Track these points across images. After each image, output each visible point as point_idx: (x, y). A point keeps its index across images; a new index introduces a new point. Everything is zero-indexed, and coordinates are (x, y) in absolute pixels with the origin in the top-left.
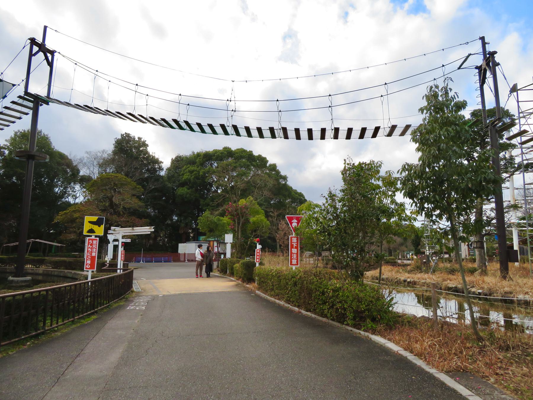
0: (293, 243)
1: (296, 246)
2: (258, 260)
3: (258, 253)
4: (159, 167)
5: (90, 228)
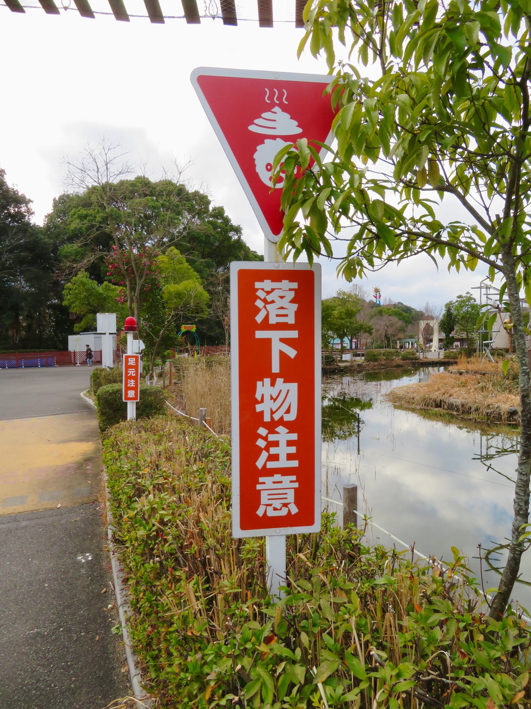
0: (266, 325)
1: (292, 353)
2: (131, 393)
3: (131, 367)
4: (28, 209)
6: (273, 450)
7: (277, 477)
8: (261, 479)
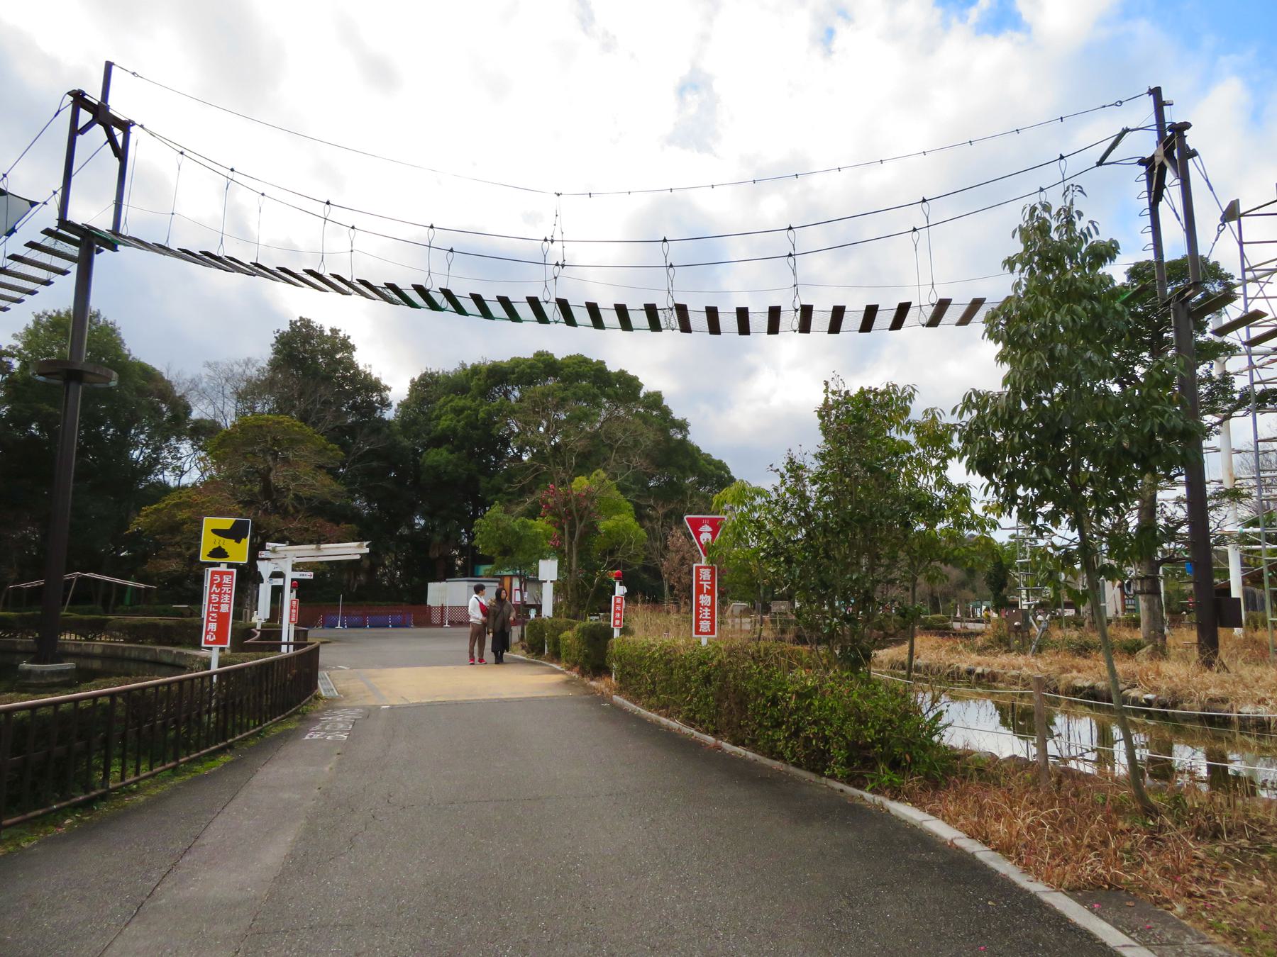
0: (702, 580)
1: (709, 588)
2: (618, 622)
3: (618, 604)
4: (382, 398)
5: (216, 546)
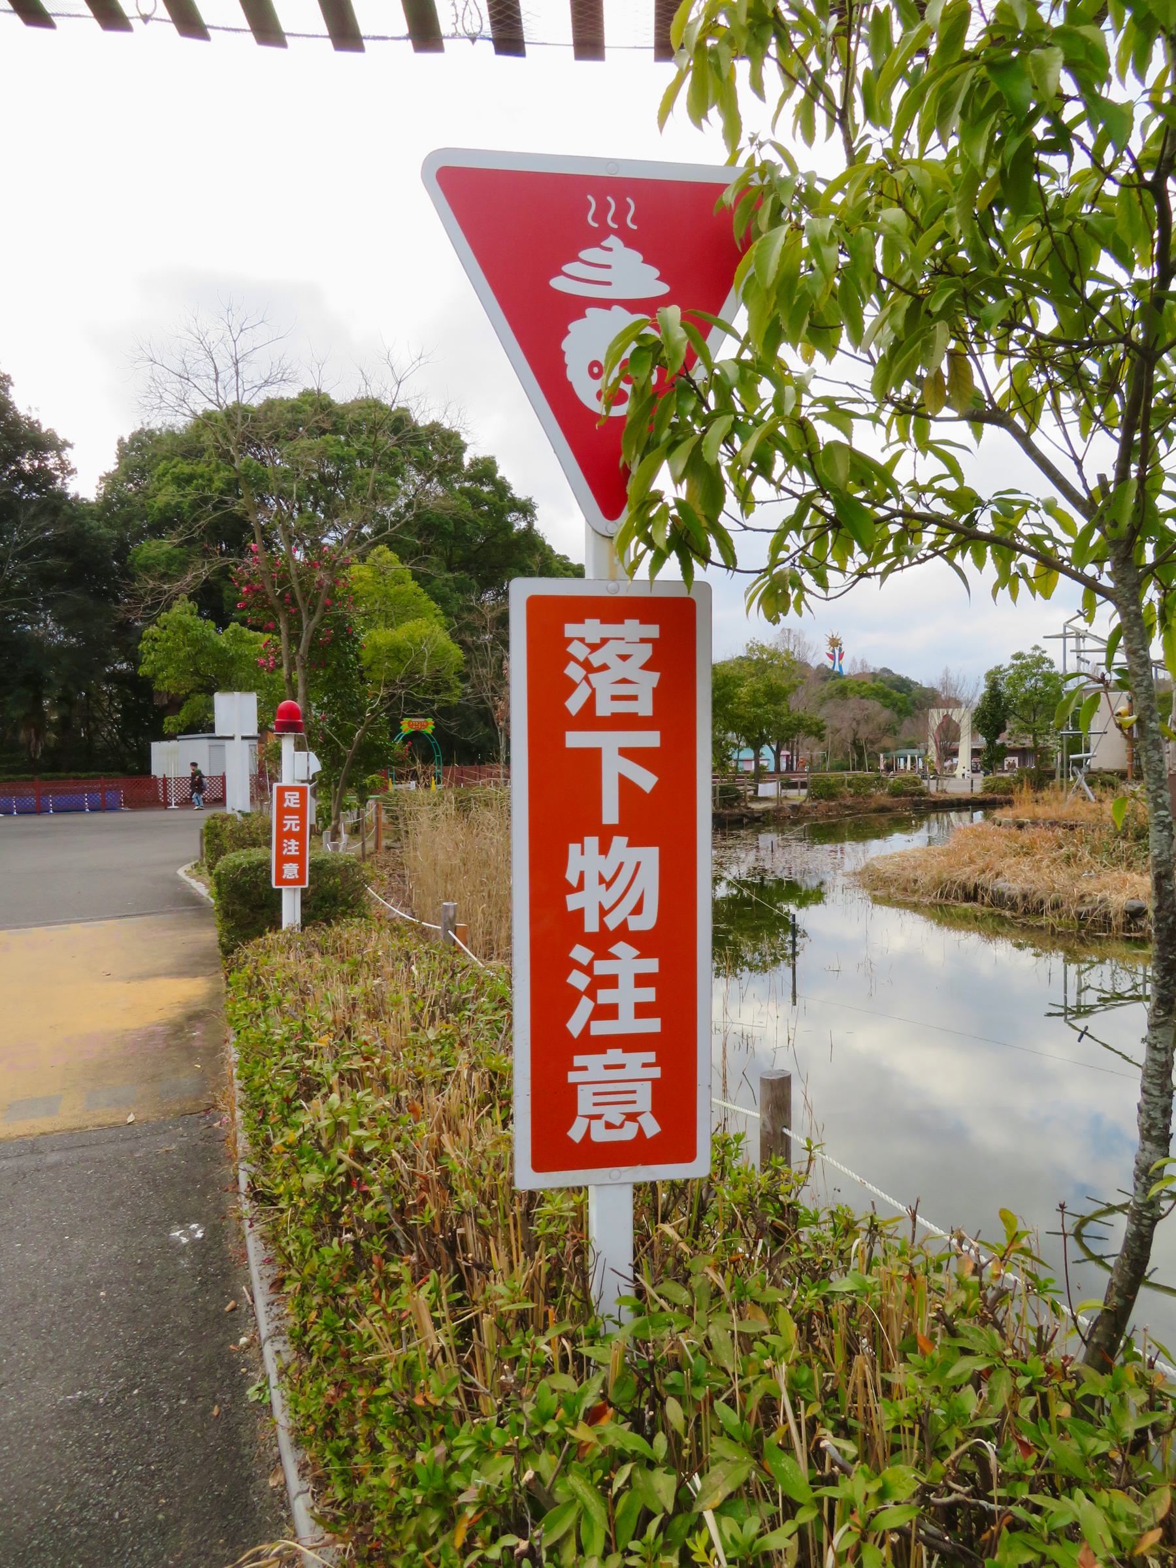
0: (588, 719)
1: (646, 780)
2: (291, 870)
3: (291, 811)
4: (63, 462)
6: (605, 996)
7: (615, 1055)
8: (578, 1060)
